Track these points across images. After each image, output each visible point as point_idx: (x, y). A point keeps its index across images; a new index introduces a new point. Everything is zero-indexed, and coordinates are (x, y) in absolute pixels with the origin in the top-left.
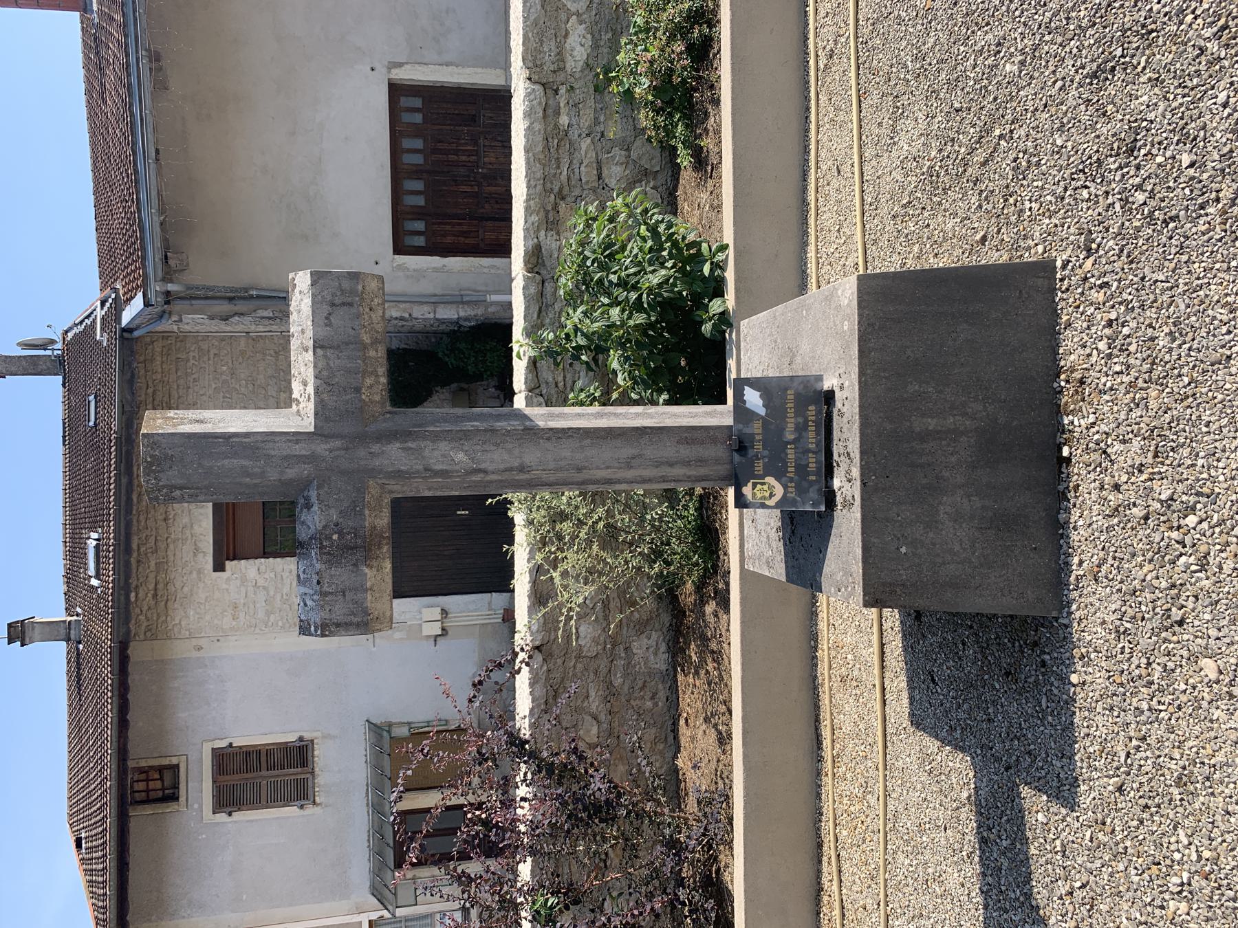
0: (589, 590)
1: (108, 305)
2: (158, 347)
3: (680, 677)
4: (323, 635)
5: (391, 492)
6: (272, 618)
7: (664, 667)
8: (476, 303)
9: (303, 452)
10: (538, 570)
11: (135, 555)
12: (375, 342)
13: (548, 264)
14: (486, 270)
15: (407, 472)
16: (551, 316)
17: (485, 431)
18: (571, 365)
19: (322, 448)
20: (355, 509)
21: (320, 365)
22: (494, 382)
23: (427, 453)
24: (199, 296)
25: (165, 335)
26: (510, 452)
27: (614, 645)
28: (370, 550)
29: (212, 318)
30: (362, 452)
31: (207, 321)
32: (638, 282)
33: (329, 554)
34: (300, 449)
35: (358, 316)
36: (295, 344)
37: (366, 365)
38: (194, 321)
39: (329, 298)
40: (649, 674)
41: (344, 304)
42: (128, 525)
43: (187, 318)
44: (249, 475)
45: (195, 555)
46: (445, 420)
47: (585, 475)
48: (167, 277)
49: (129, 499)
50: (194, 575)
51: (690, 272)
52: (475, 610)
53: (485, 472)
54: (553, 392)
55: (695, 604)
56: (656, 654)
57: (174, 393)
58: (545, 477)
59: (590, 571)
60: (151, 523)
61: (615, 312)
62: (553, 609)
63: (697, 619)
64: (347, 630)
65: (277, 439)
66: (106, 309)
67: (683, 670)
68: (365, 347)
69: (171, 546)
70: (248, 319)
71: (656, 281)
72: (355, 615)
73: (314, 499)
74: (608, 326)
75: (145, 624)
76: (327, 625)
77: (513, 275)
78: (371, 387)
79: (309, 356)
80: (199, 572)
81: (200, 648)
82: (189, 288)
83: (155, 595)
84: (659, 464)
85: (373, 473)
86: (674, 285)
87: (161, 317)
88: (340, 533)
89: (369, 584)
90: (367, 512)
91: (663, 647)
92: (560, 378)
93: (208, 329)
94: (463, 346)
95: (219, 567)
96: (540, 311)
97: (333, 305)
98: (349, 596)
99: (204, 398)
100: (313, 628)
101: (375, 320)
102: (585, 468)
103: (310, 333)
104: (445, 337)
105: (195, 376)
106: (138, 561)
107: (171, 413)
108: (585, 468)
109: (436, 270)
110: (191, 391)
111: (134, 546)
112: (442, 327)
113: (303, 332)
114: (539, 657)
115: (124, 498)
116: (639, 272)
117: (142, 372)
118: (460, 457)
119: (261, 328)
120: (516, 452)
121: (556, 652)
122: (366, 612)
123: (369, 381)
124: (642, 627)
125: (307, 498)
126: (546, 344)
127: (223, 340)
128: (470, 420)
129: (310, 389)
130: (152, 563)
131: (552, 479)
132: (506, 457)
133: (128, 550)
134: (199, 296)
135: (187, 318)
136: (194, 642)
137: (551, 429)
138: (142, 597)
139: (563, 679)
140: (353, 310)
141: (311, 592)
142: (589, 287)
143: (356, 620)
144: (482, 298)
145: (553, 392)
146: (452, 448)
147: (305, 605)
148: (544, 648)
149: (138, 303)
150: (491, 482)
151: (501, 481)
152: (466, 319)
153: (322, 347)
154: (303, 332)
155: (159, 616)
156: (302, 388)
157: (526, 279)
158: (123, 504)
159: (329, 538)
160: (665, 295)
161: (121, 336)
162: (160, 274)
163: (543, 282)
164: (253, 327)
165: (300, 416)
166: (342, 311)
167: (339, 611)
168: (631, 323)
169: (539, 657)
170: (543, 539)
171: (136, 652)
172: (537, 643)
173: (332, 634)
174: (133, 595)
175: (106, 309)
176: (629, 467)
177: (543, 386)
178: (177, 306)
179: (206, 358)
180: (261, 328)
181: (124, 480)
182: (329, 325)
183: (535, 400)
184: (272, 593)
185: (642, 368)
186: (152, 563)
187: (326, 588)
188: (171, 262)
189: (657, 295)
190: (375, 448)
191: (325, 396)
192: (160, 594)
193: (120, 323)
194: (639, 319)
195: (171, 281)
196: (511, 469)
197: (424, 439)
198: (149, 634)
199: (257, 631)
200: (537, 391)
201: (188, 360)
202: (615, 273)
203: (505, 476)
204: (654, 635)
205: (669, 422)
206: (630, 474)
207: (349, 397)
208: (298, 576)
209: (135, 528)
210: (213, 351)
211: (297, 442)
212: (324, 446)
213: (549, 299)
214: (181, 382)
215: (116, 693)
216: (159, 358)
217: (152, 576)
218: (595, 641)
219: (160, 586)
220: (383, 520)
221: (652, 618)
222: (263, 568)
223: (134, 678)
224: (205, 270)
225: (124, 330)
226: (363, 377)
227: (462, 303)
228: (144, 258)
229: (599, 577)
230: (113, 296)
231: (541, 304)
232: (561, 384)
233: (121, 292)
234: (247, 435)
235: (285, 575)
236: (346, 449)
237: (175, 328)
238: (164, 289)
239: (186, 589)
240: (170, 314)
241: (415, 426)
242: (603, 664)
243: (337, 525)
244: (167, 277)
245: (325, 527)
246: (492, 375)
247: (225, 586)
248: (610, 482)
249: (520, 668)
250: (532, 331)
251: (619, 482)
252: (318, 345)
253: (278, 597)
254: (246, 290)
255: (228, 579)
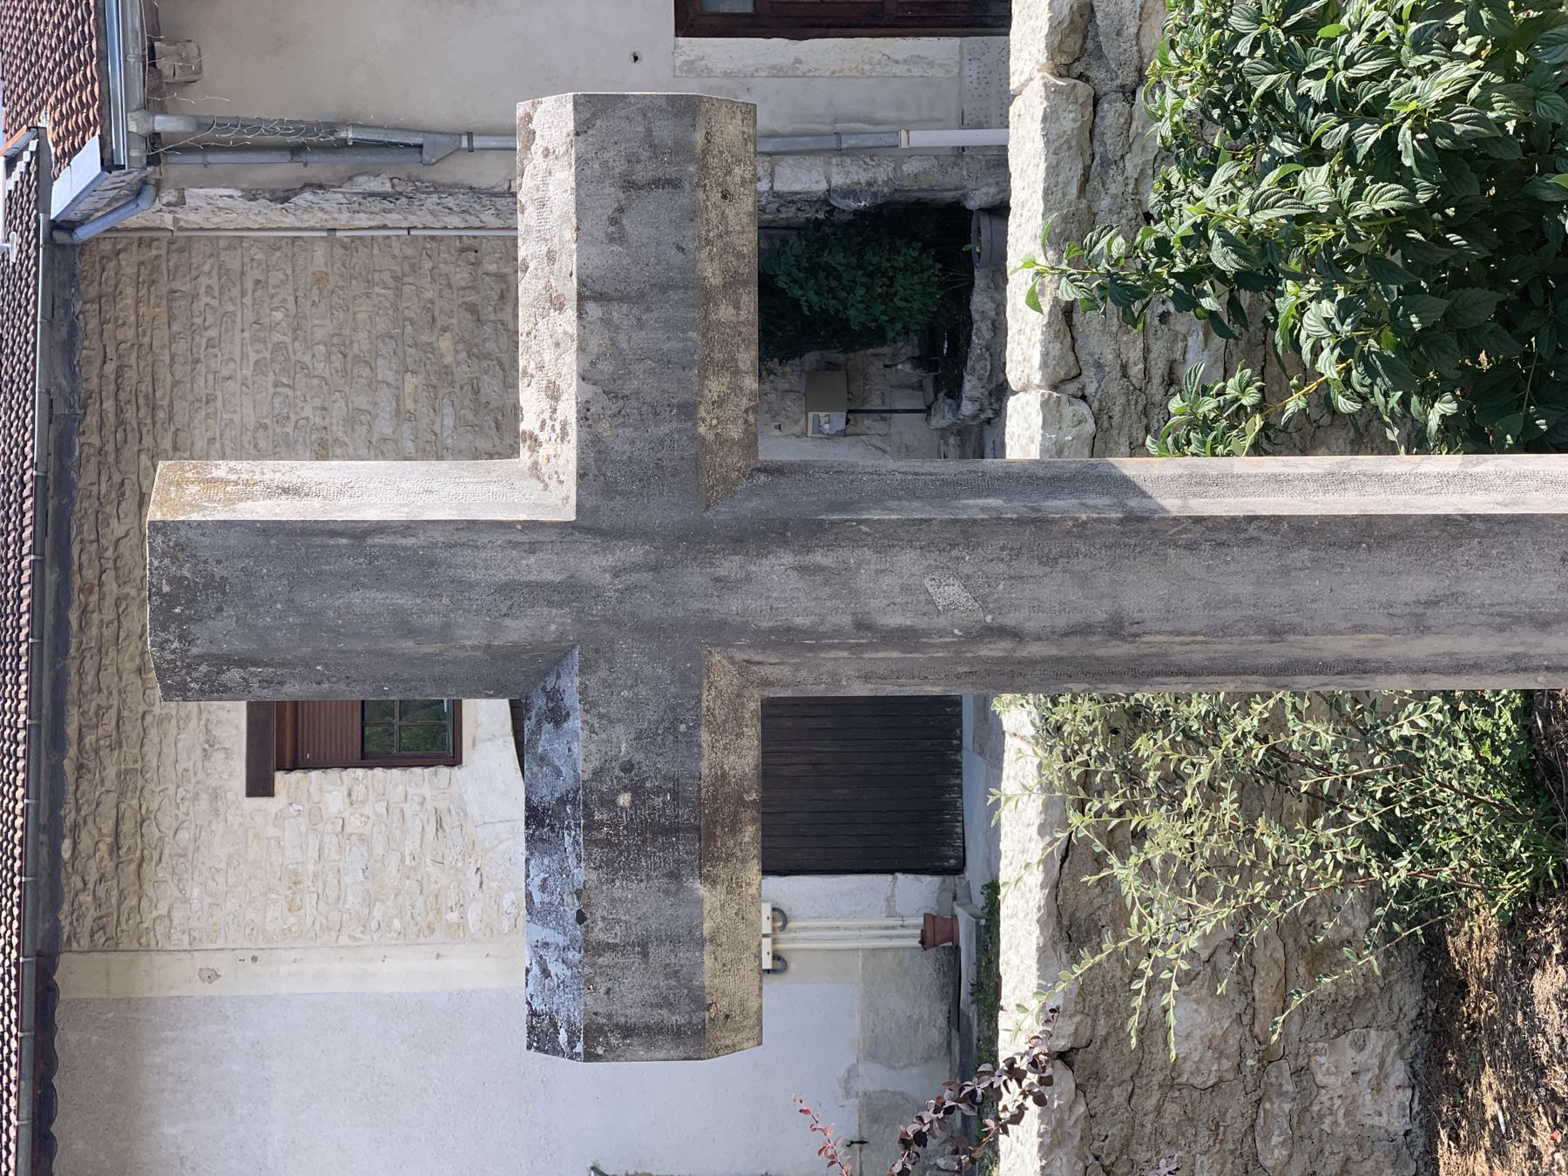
0: (1213, 917)
1: (20, 166)
2: (128, 264)
3: (1443, 1153)
4: (590, 1056)
5: (766, 683)
6: (378, 912)
7: (1399, 1125)
8: (872, 152)
9: (548, 576)
10: (1068, 859)
11: (72, 751)
12: (732, 282)
13: (1110, 52)
14: (899, 70)
15: (807, 633)
16: (1114, 189)
17: (1020, 522)
18: (1164, 317)
19: (594, 565)
20: (675, 726)
21: (594, 347)
22: (910, 348)
23: (862, 580)
24: (219, 143)
25: (146, 237)
26: (1083, 580)
27: (1262, 1065)
28: (712, 837)
29: (251, 196)
30: (695, 577)
31: (241, 204)
32: (1384, 98)
33: (607, 843)
34: (541, 568)
35: (693, 214)
36: (528, 289)
37: (709, 343)
38: (211, 203)
39: (620, 167)
40: (1359, 1141)
41: (658, 183)
42: (60, 682)
43: (195, 195)
44: (410, 631)
45: (206, 755)
46: (909, 491)
47: (1294, 648)
48: (155, 100)
49: (62, 623)
50: (204, 803)
51: (1525, 69)
52: (855, 915)
53: (1016, 635)
54: (1114, 389)
55: (1500, 967)
56: (1377, 1089)
57: (164, 373)
58: (1179, 652)
59: (1221, 864)
60: (108, 678)
61: (1316, 183)
62: (1117, 956)
63: (1507, 1009)
64: (650, 1045)
65: (484, 539)
66: (16, 176)
67: (1454, 1137)
68: (707, 297)
69: (153, 734)
70: (335, 197)
71: (1437, 94)
72: (670, 1005)
73: (572, 699)
74: (1299, 220)
75: (92, 914)
76: (600, 1030)
77: (1014, 83)
78: (720, 403)
79: (567, 321)
80: (215, 796)
81: (213, 976)
82: (201, 125)
83: (116, 847)
84: (1505, 621)
85: (720, 632)
86: (1484, 103)
87: (138, 194)
88: (637, 791)
89: (707, 927)
90: (705, 737)
91: (1399, 1073)
92: (1135, 354)
93: (242, 221)
94: (837, 258)
95: (260, 785)
96: (1086, 178)
97: (630, 185)
98: (658, 954)
99: (231, 386)
100: (563, 1037)
101: (734, 225)
102: (1293, 630)
103: (569, 261)
104: (793, 239)
105: (213, 333)
106: (80, 767)
107: (220, 469)
108: (1293, 630)
109: (777, 72)
110: (201, 368)
111: (72, 731)
112: (788, 213)
113: (551, 257)
114: (1065, 1082)
115: (49, 618)
116: (1383, 74)
117: (93, 324)
118: (951, 592)
119: (363, 220)
120: (1103, 580)
121: (1111, 1069)
122: (699, 1001)
123: (715, 387)
124: (1341, 1016)
125: (554, 696)
126: (1104, 266)
127: (274, 247)
128: (978, 492)
129: (568, 409)
130: (111, 773)
131: (1199, 655)
132: (1074, 595)
133: (57, 740)
134: (219, 143)
135: (195, 195)
136: (200, 960)
137: (1198, 520)
138: (88, 850)
139: (1126, 1145)
140: (682, 200)
141: (561, 940)
142: (1240, 116)
143: (676, 1019)
144: (889, 140)
145: (1114, 389)
146: (929, 570)
147: (546, 973)
148: (1078, 1058)
149: (88, 162)
150: (1031, 662)
151: (1058, 660)
152: (849, 192)
153: (600, 298)
154: (551, 257)
155: (122, 896)
156: (546, 404)
157: (1052, 93)
158: (48, 632)
159: (609, 802)
160: (1459, 129)
161: (50, 239)
162: (138, 93)
163: (1096, 101)
164: (344, 218)
165: (538, 482)
166: (653, 202)
167: (632, 994)
168: (1362, 209)
169: (1065, 1082)
170: (1086, 778)
171: (78, 976)
172: (1062, 1044)
173: (612, 1054)
174: (67, 844)
175: (16, 176)
176: (1420, 627)
177: (1089, 373)
178: (175, 169)
179: (236, 291)
180: (363, 220)
181: (52, 577)
182: (619, 237)
183: (1068, 411)
184: (379, 850)
185: (1388, 333)
186: (111, 773)
187: (598, 934)
188: (161, 63)
189: (1434, 132)
190: (729, 566)
191: (604, 428)
192: (126, 843)
193: (47, 211)
194: (1384, 198)
195: (162, 110)
196: (1084, 630)
197: (857, 541)
198: (100, 938)
199: (344, 940)
200: (1073, 387)
201: (195, 297)
202: (1318, 74)
203: (1071, 647)
204: (1376, 1040)
205: (1538, 503)
206: (1421, 648)
207: (664, 429)
208: (529, 896)
209: (73, 689)
210: (254, 274)
211: (533, 548)
212: (608, 561)
213: (1110, 142)
214: (181, 347)
215: (27, 1071)
216: (130, 291)
217: (109, 801)
218: (1214, 1046)
219: (128, 826)
220: (738, 757)
221: (1369, 994)
222: (359, 791)
223: (68, 1038)
224: (238, 81)
225: (55, 225)
226: (703, 377)
227: (840, 152)
228: (103, 57)
229: (1244, 883)
230: (33, 146)
231: (1087, 159)
232: (1136, 370)
233: (51, 136)
234: (409, 527)
235: (410, 809)
236: (656, 568)
237: (168, 219)
238: (146, 128)
239: (184, 835)
240: (158, 186)
241: (834, 507)
242: (1236, 1107)
243: (628, 767)
244: (155, 100)
245: (598, 773)
246: (906, 330)
247: (271, 831)
248: (1359, 667)
249: (1022, 1109)
250: (1070, 232)
251: (1387, 669)
252: (589, 293)
253: (394, 859)
254: (332, 128)
255: (279, 817)
